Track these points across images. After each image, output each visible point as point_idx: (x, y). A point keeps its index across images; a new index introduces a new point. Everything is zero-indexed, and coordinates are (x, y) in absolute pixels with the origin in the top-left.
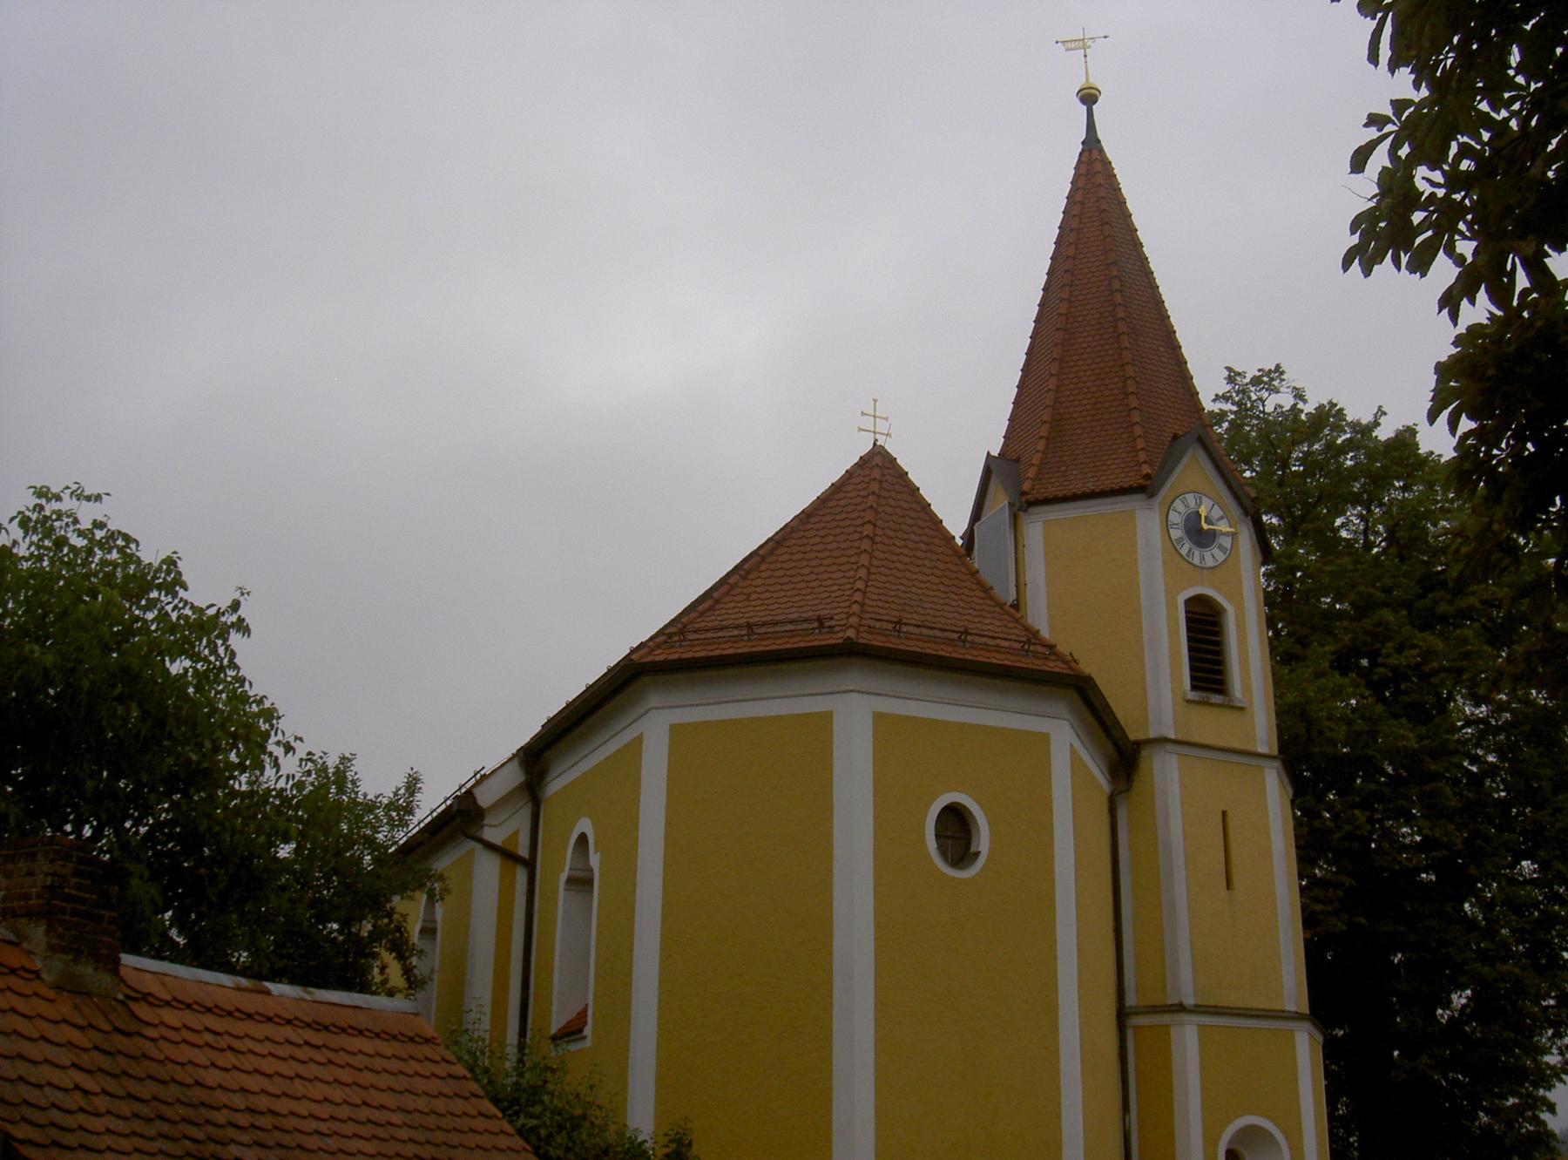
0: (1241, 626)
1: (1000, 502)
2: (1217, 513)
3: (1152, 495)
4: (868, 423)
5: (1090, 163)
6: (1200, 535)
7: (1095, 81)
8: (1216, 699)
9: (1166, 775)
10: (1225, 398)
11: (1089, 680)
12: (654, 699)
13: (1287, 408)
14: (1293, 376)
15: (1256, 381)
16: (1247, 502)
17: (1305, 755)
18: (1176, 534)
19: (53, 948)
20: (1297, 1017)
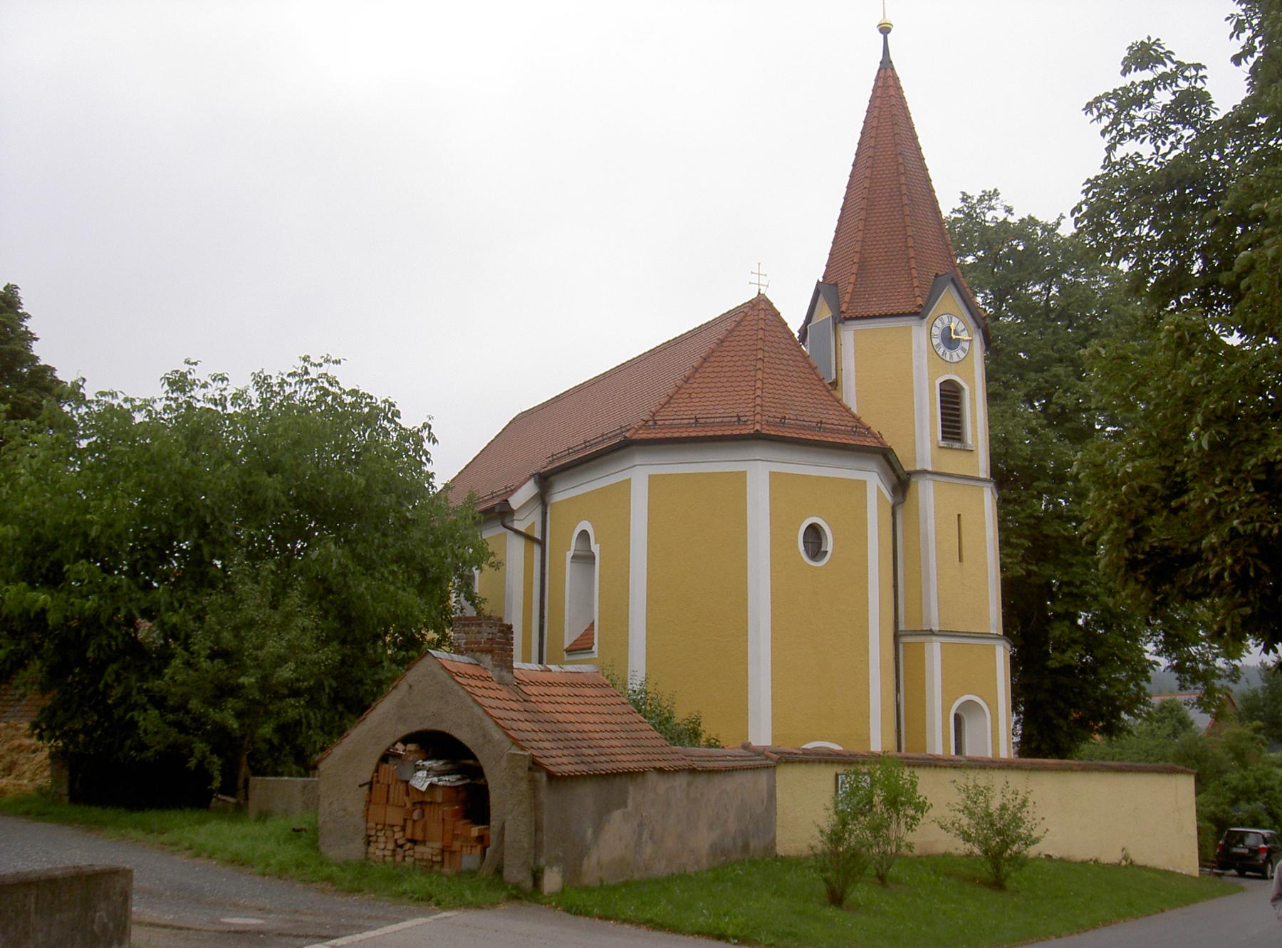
0: (973, 400)
1: (824, 313)
2: (961, 327)
3: (923, 318)
4: (755, 279)
5: (886, 78)
6: (950, 341)
7: (890, 19)
8: (957, 445)
9: (926, 493)
10: (959, 211)
11: (890, 450)
12: (638, 459)
13: (1001, 219)
14: (1005, 198)
15: (981, 200)
16: (981, 322)
17: (1010, 476)
18: (936, 341)
19: (495, 666)
20: (997, 637)
